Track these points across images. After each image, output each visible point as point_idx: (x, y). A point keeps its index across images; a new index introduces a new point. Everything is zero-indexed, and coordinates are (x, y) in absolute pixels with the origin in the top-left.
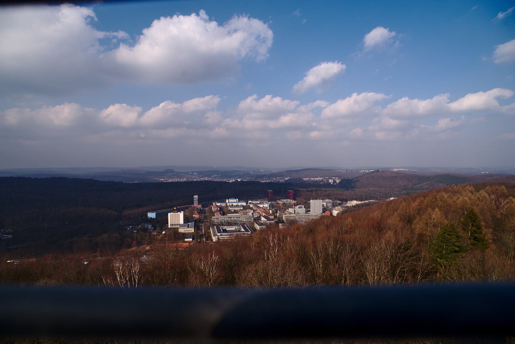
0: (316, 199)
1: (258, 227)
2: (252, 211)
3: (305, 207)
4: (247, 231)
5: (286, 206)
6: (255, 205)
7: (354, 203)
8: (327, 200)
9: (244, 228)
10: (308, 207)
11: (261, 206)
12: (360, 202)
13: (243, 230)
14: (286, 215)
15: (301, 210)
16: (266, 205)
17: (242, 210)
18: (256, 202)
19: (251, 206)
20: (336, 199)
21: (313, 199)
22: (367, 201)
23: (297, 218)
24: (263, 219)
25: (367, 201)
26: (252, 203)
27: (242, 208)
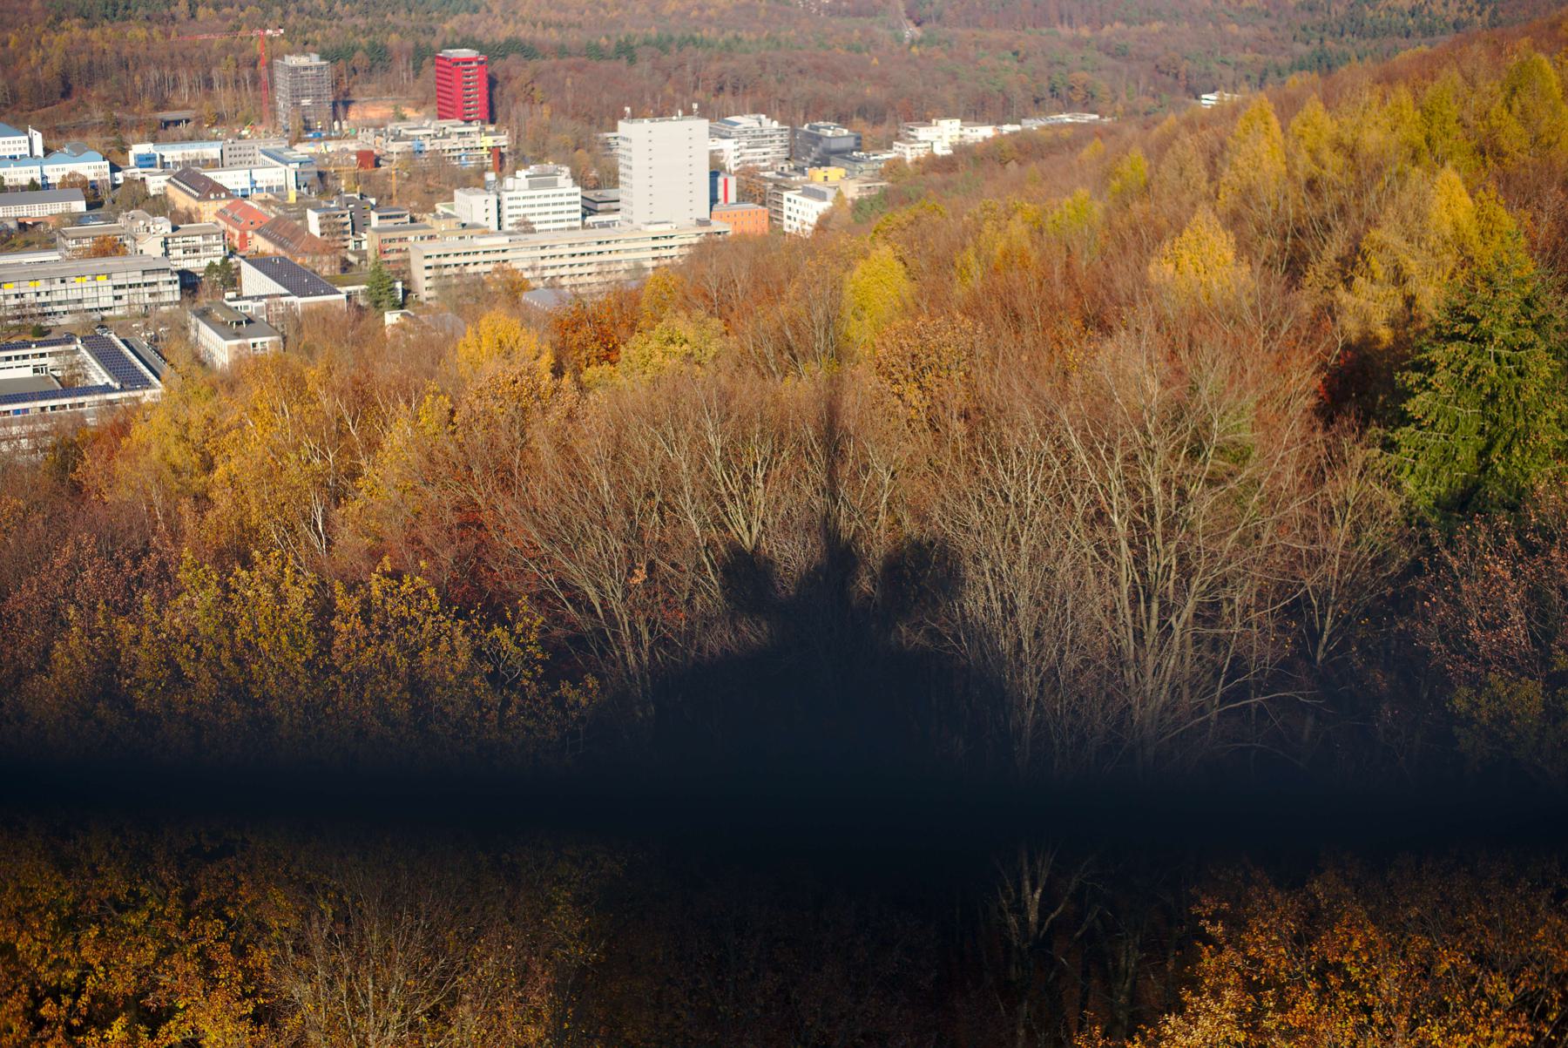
0: (662, 113)
1: (220, 350)
2: (163, 226)
3: (578, 178)
4: (130, 379)
5: (437, 180)
6: (192, 177)
7: (942, 136)
8: (746, 121)
9: (109, 358)
10: (599, 185)
11: (234, 179)
12: (983, 132)
13: (98, 375)
14: (433, 248)
15: (544, 198)
16: (277, 175)
17: (78, 219)
18: (193, 151)
19: (156, 183)
20: (817, 108)
21: (634, 116)
22: (1033, 124)
23: (520, 260)
24: (254, 281)
25: (1033, 124)
26: (155, 162)
27: (80, 206)
